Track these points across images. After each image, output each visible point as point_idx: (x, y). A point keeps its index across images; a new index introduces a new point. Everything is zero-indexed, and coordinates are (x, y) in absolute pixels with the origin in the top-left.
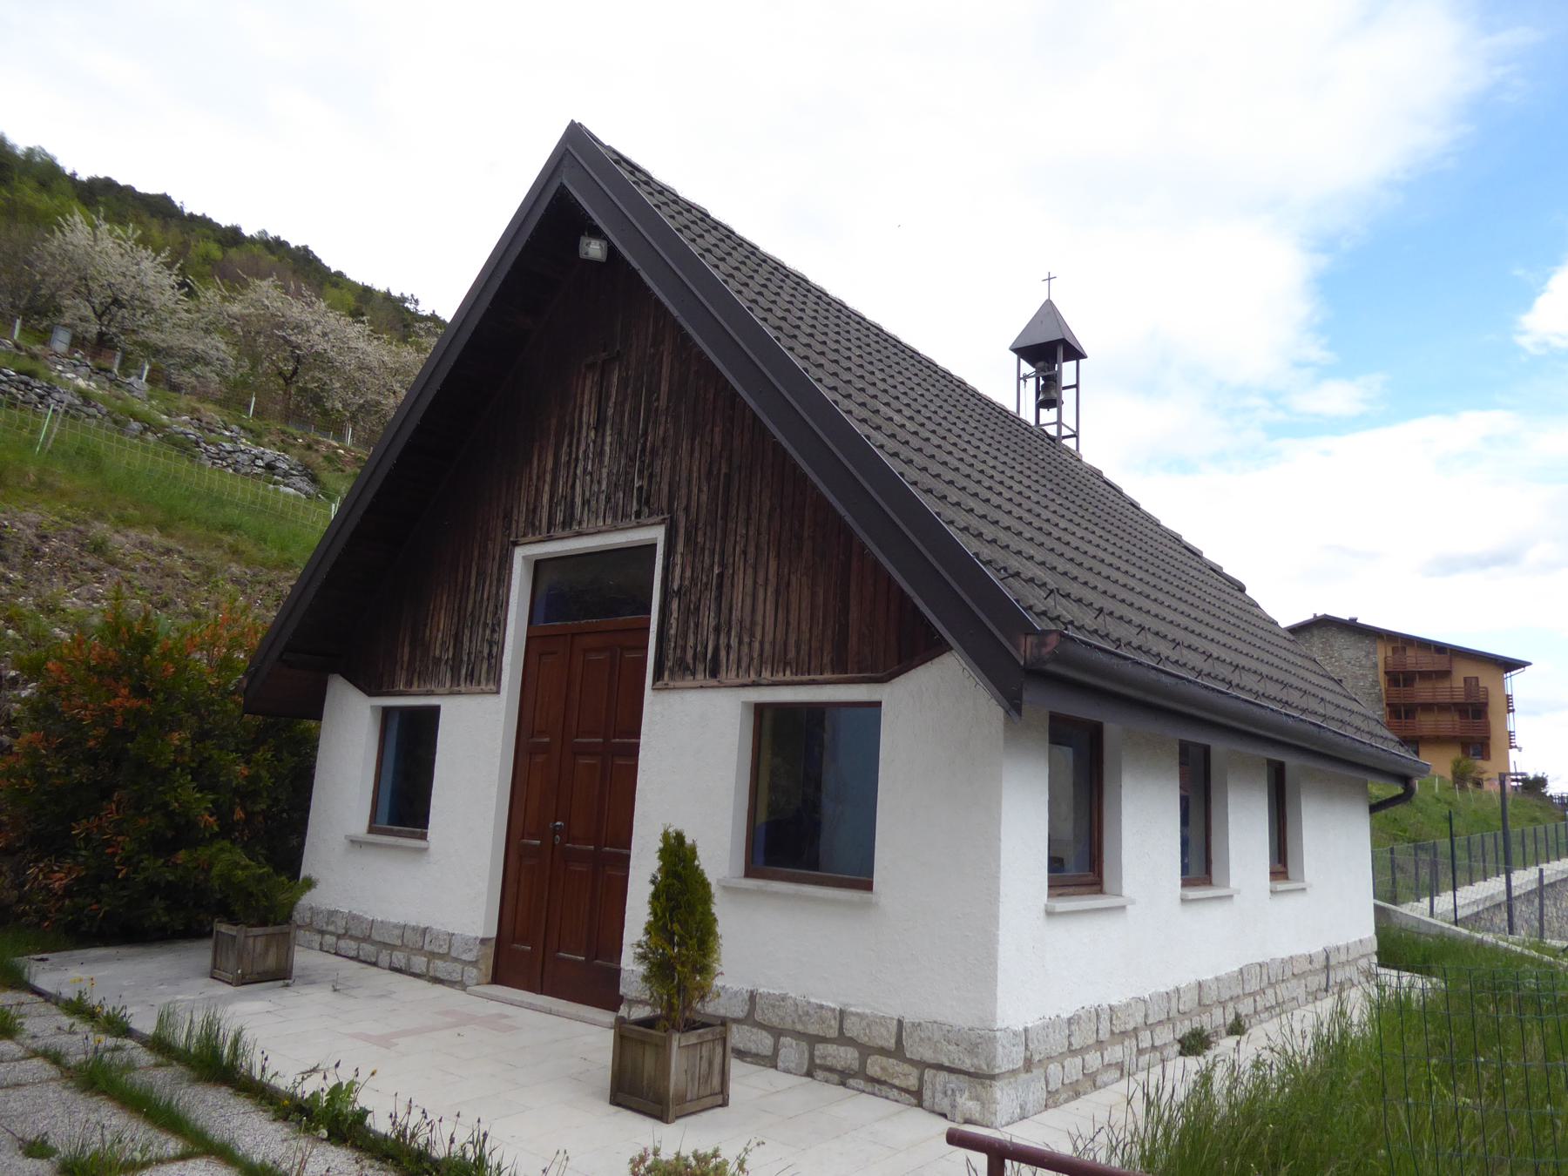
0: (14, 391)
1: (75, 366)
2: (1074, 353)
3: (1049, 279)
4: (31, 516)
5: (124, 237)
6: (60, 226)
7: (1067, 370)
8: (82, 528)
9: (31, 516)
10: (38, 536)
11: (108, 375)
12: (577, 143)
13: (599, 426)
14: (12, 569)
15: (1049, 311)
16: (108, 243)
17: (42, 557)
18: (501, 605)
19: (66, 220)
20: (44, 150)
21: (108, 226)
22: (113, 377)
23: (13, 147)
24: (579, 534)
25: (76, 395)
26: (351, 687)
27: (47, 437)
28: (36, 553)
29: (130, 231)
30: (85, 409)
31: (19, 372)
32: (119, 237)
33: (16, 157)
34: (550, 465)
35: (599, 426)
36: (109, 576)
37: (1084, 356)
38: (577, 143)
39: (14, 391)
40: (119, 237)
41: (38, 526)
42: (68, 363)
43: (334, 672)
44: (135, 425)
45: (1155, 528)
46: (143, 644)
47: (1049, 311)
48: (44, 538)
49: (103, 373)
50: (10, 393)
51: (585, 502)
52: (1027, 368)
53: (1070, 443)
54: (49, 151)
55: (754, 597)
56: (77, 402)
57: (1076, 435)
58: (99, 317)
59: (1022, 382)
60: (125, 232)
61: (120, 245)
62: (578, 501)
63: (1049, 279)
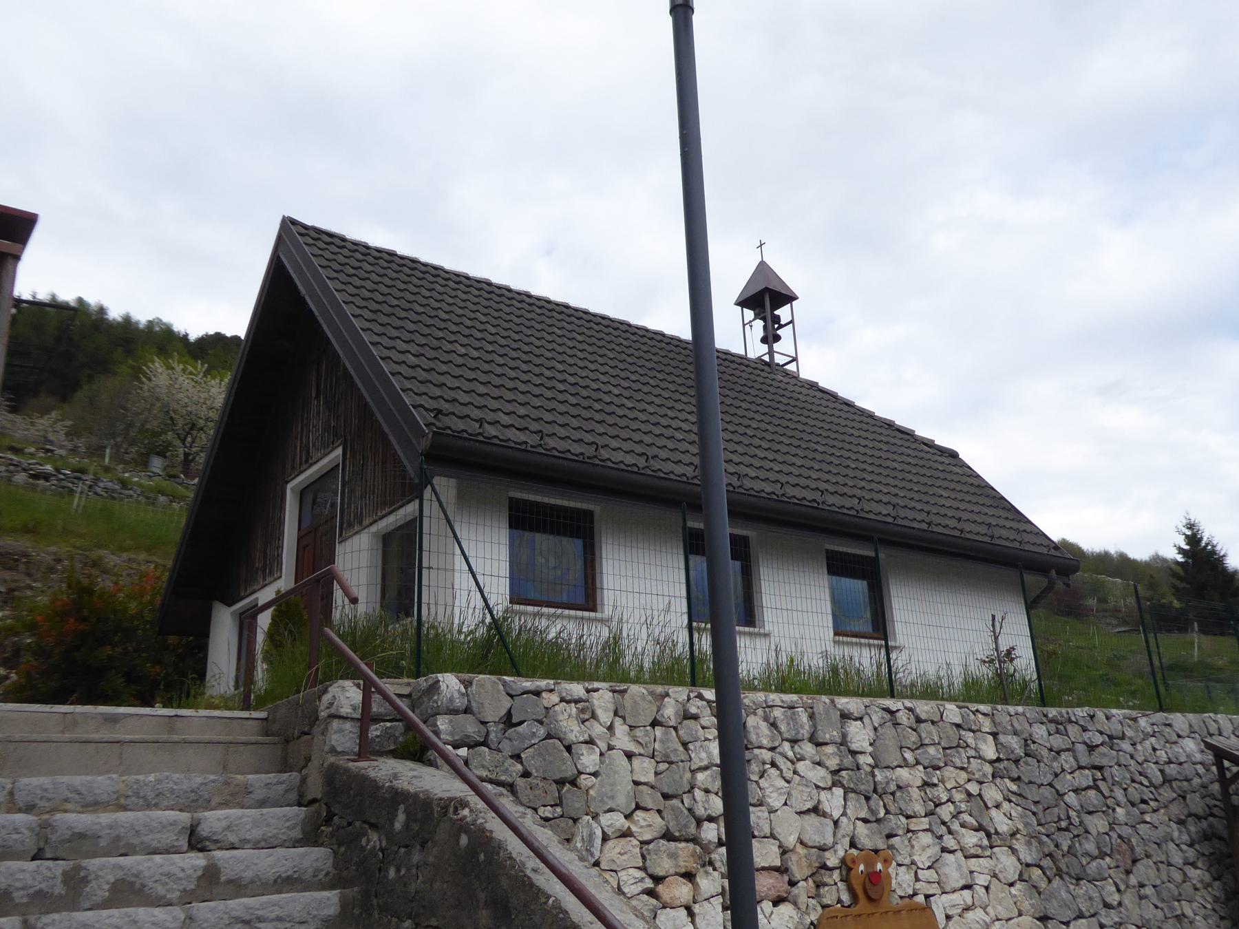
0: (70, 485)
1: (150, 477)
2: (787, 298)
3: (761, 245)
4: (53, 549)
5: (194, 372)
6: (145, 374)
7: (784, 313)
8: (87, 553)
9: (53, 549)
10: (55, 560)
11: (177, 480)
12: (290, 228)
13: (317, 397)
14: (35, 581)
15: (763, 268)
16: (185, 382)
17: (57, 572)
18: (281, 522)
19: (148, 367)
20: (161, 320)
21: (181, 366)
22: (180, 481)
23: (137, 323)
24: (311, 465)
25: (116, 482)
26: (225, 606)
27: (78, 505)
28: (52, 570)
29: (199, 366)
30: (124, 491)
31: (73, 471)
32: (191, 373)
33: (137, 329)
34: (300, 428)
35: (317, 397)
36: (103, 580)
37: (795, 298)
38: (290, 228)
39: (70, 485)
40: (191, 373)
41: (55, 554)
42: (144, 476)
43: (217, 599)
44: (162, 499)
45: (869, 420)
46: (88, 591)
47: (763, 268)
48: (59, 561)
49: (172, 479)
50: (69, 487)
51: (314, 444)
52: (749, 314)
53: (792, 367)
54: (165, 320)
55: (374, 470)
56: (117, 487)
57: (795, 359)
58: (183, 441)
59: (747, 327)
60: (196, 368)
61: (192, 379)
62: (311, 445)
63: (761, 245)
